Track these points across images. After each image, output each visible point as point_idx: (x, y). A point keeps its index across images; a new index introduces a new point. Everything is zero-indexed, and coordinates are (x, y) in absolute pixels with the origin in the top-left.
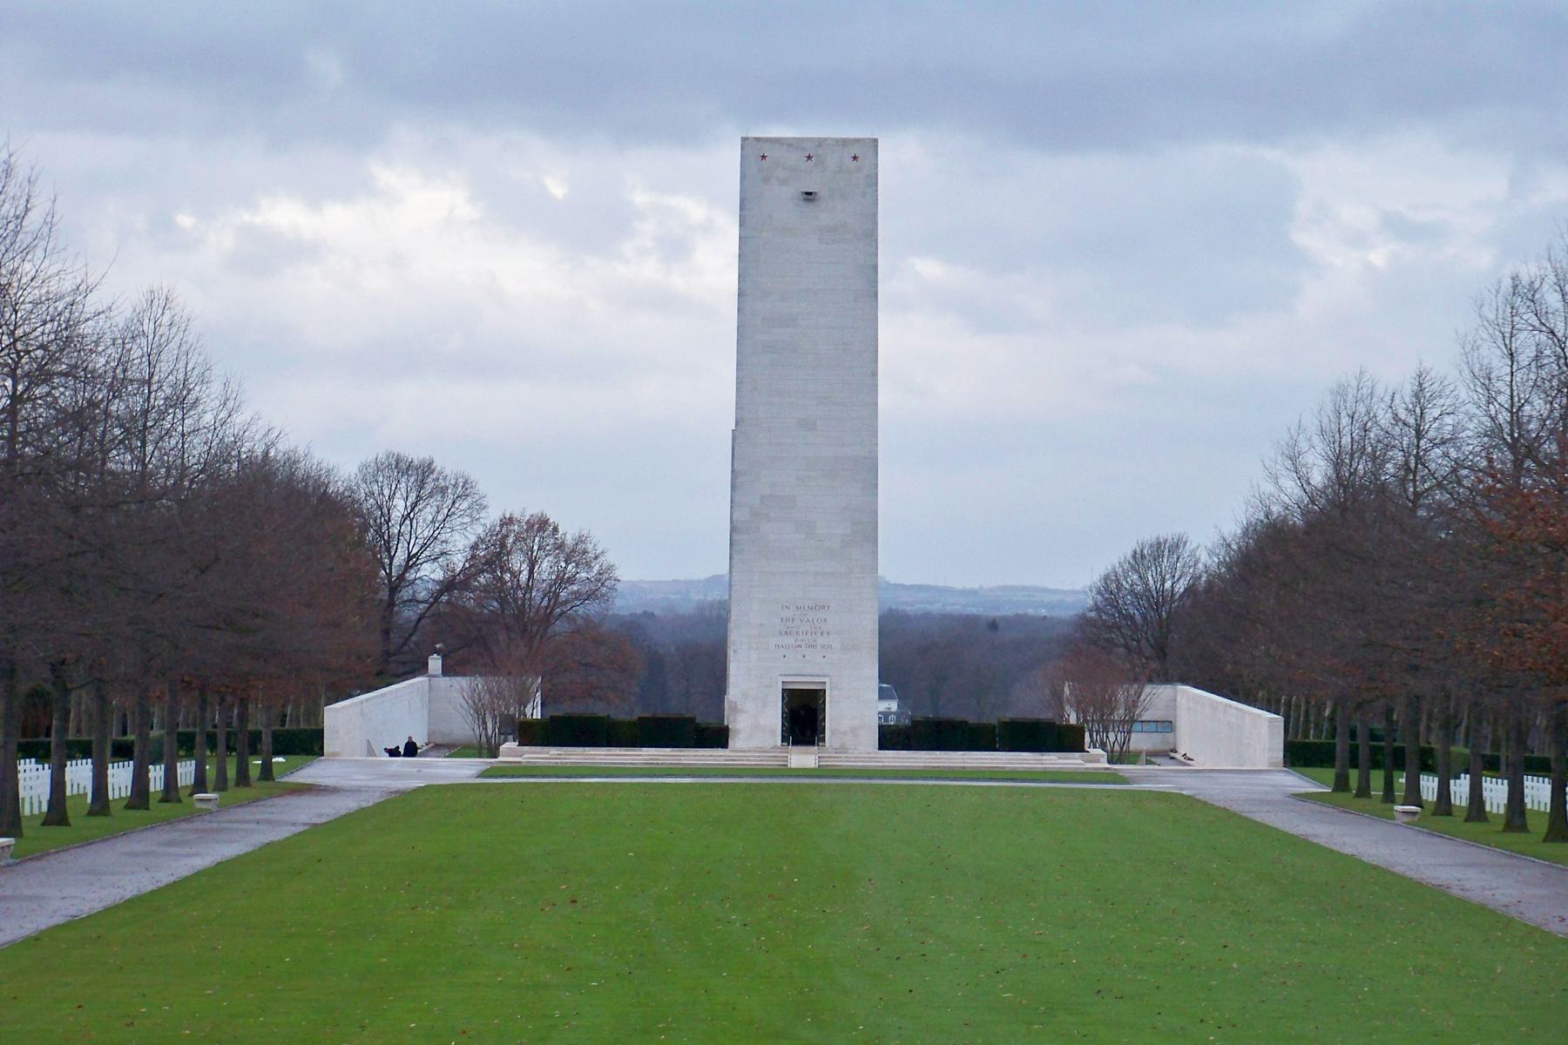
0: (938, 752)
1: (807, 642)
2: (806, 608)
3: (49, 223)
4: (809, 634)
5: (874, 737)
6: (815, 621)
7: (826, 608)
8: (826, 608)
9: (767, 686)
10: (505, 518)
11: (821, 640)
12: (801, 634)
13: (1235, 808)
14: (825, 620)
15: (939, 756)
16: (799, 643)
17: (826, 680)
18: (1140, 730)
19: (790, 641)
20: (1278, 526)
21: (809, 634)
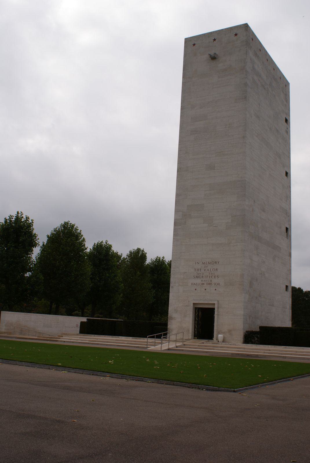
0: (270, 346)
1: (207, 282)
2: (207, 263)
3: (10, 215)
4: (208, 278)
5: (241, 337)
6: (212, 270)
7: (217, 263)
8: (217, 263)
9: (187, 306)
10: (91, 250)
11: (215, 281)
12: (204, 278)
13: (153, 349)
14: (217, 269)
15: (270, 349)
16: (203, 282)
17: (216, 302)
18: (48, 368)
19: (198, 281)
20: (28, 276)
21: (208, 278)
